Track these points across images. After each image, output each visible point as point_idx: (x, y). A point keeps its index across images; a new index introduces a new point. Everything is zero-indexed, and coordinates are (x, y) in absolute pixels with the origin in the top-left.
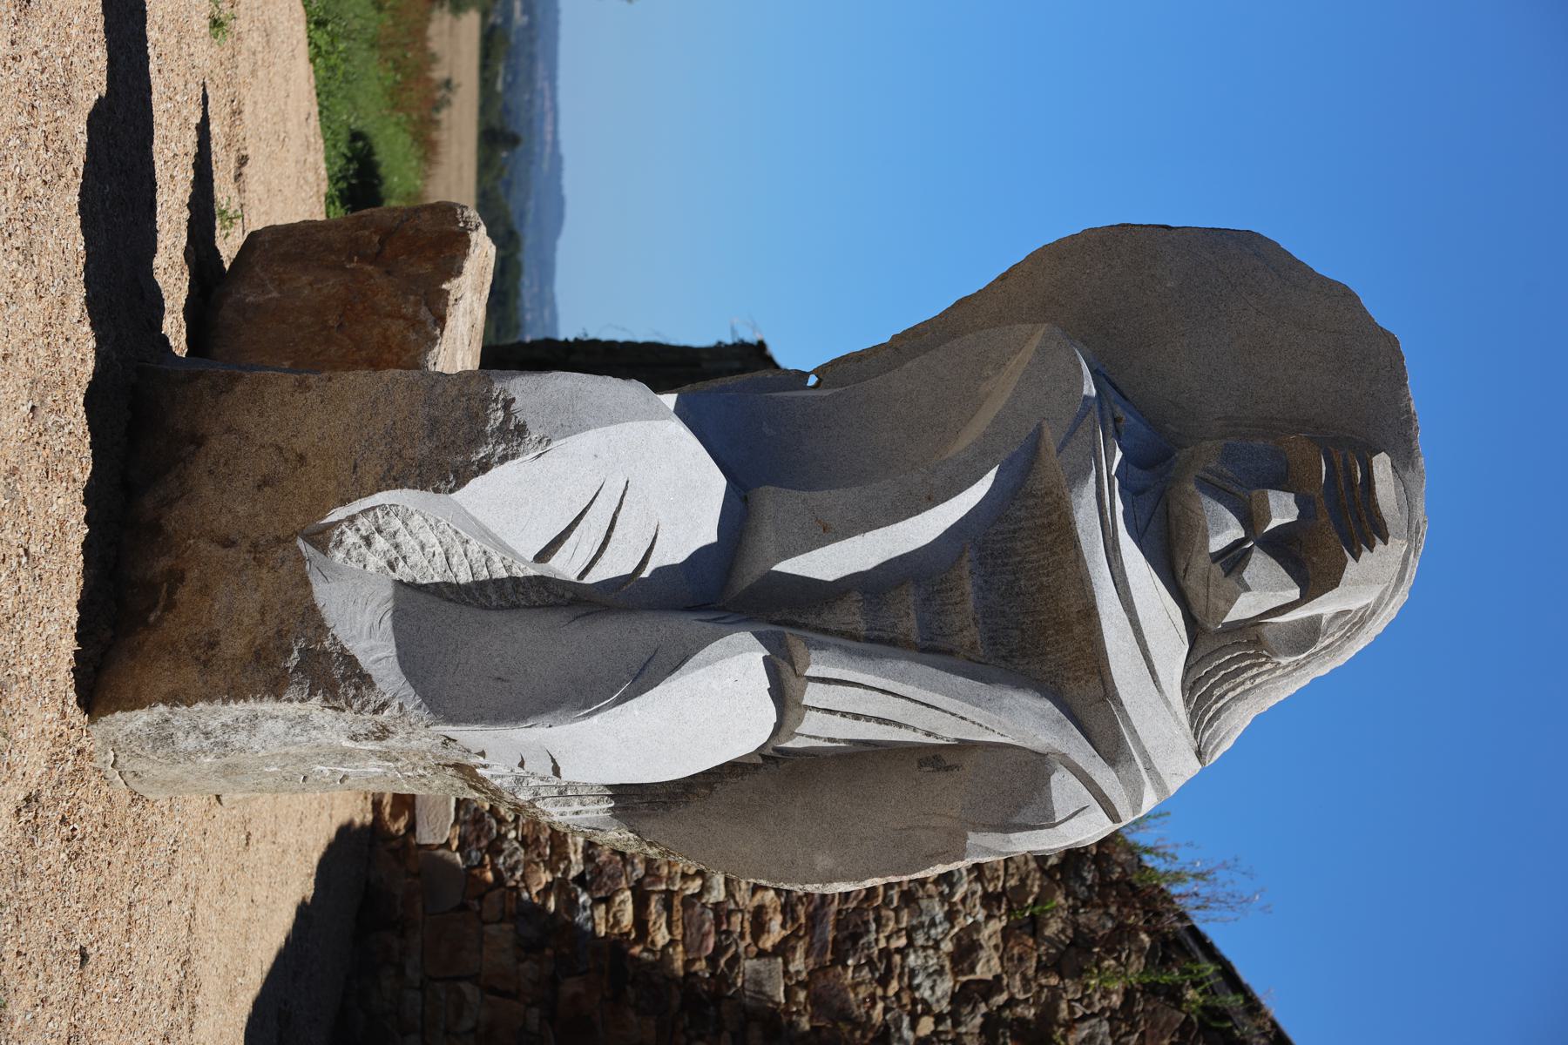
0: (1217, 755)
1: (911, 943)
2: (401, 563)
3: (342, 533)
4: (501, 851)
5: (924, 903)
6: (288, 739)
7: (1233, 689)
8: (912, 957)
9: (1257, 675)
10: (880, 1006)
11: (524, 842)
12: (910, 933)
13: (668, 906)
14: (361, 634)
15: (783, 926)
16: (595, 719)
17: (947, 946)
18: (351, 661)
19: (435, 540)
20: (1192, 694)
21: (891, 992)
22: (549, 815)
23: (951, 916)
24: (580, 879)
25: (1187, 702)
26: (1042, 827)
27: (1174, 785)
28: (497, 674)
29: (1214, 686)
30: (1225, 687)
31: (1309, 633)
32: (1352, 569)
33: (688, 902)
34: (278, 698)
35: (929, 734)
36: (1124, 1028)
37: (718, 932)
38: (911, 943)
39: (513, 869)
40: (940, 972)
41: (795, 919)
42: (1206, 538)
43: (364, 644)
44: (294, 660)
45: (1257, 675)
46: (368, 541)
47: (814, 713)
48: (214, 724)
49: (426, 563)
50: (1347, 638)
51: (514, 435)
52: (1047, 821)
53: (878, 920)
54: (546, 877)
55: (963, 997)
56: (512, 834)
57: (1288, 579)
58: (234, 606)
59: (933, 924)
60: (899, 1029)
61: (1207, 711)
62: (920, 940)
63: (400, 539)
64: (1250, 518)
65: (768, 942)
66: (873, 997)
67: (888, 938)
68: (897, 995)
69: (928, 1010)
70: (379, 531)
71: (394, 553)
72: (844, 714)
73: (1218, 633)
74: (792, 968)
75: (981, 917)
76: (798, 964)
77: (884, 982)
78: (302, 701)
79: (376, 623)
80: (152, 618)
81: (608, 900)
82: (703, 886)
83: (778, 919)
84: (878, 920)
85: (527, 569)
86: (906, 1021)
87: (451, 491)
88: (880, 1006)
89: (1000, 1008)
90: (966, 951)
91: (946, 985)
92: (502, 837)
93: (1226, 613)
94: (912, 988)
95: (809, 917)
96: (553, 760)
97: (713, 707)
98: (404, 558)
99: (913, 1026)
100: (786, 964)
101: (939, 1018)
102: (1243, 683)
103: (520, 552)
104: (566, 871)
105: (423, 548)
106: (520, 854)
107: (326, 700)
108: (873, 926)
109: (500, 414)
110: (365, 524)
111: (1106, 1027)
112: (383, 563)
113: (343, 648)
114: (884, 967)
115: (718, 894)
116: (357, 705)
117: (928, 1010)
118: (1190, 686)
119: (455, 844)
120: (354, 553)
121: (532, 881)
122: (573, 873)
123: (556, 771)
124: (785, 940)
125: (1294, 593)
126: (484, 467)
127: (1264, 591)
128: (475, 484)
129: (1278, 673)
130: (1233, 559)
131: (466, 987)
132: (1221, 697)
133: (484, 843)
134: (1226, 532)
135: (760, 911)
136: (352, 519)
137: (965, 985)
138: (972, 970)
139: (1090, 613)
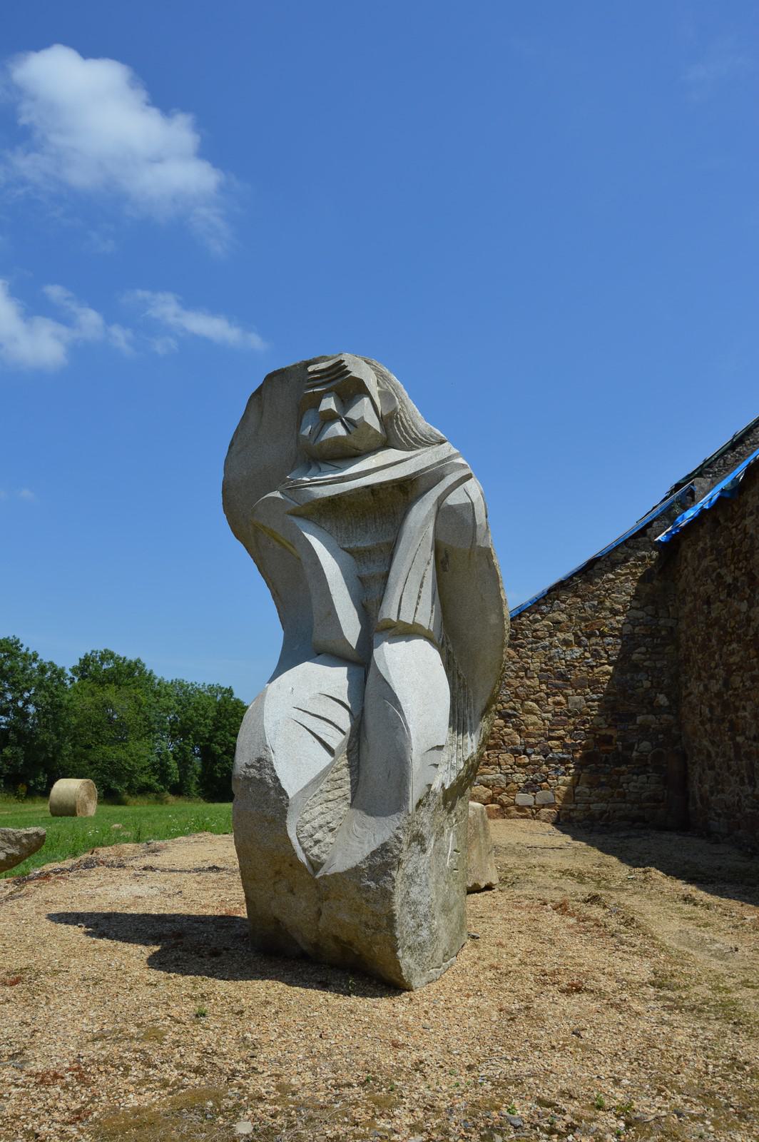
0: (442, 435)
1: (564, 659)
2: (331, 825)
3: (312, 855)
4: (536, 780)
5: (552, 655)
6: (424, 884)
7: (412, 429)
8: (568, 659)
9: (406, 419)
10: (582, 668)
11: (534, 773)
12: (561, 659)
13: (553, 731)
14: (361, 848)
15: (559, 696)
16: (410, 726)
17: (564, 648)
18: (374, 854)
19: (319, 807)
20: (414, 446)
21: (578, 665)
22: (473, 753)
23: (556, 647)
24: (545, 756)
25: (418, 448)
26: (473, 509)
27: (455, 451)
28: (387, 777)
29: (411, 437)
30: (411, 432)
32: (355, 374)
33: (552, 725)
34: (392, 894)
35: (429, 563)
36: (587, 598)
37: (561, 715)
38: (564, 659)
39: (542, 777)
40: (572, 650)
41: (557, 693)
43: (366, 847)
44: (372, 884)
45: (406, 419)
46: (317, 842)
47: (416, 618)
48: (412, 923)
49: (332, 812)
50: (390, 381)
51: (263, 763)
52: (471, 507)
53: (557, 668)
54: (544, 767)
55: (579, 644)
56: (531, 777)
57: (362, 400)
58: (342, 919)
59: (558, 652)
60: (589, 663)
61: (422, 440)
62: (562, 656)
63: (316, 825)
64: (330, 418)
65: (564, 701)
66: (579, 670)
67: (562, 665)
68: (579, 663)
69: (583, 654)
70: (312, 835)
71: (325, 829)
72: (418, 604)
74: (571, 694)
75: (556, 638)
76: (570, 692)
77: (575, 667)
78: (394, 880)
79: (358, 839)
80: (357, 953)
81: (551, 748)
82: (548, 720)
83: (557, 697)
84: (557, 668)
85: (343, 759)
86: (586, 660)
87: (288, 798)
88: (582, 668)
89: (582, 633)
90: (566, 643)
91: (576, 649)
92: (532, 779)
93: (375, 430)
94: (577, 659)
95: (556, 689)
96: (433, 749)
97: (416, 674)
98: (328, 823)
99: (588, 658)
100: (569, 696)
101: (585, 651)
102: (409, 425)
103: (328, 763)
104: (543, 761)
105: (323, 813)
106: (537, 774)
107: (394, 869)
108: (559, 670)
109: (252, 770)
110: (308, 843)
111: (587, 603)
112: (330, 834)
113: (367, 858)
114: (571, 666)
115: (549, 715)
116: (396, 852)
117: (583, 654)
118: (411, 448)
119: (534, 794)
120: (324, 849)
121: (545, 771)
122: (543, 759)
123: (440, 748)
124: (563, 696)
125: (366, 400)
126: (277, 779)
127: (363, 411)
128: (284, 786)
129: (405, 410)
130: (350, 424)
131: (576, 791)
132: (415, 434)
133: (534, 785)
135: (554, 703)
136: (304, 850)
137: (575, 643)
138: (571, 641)
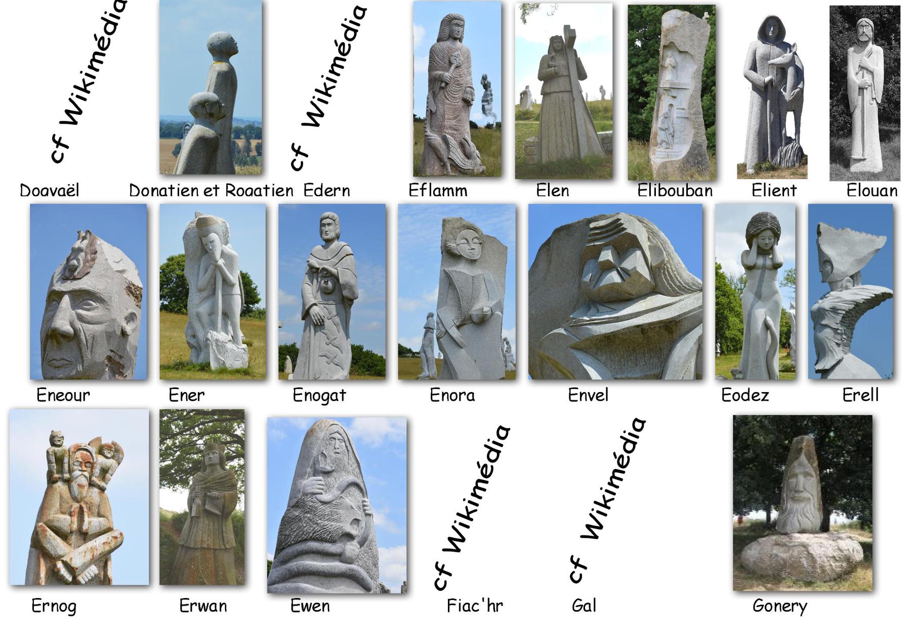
31: (654, 249)
42: (615, 284)
64: (607, 267)
73: (655, 281)
125: (639, 253)
127: (636, 262)
130: (624, 273)
134: (614, 277)
139: (642, 328)
